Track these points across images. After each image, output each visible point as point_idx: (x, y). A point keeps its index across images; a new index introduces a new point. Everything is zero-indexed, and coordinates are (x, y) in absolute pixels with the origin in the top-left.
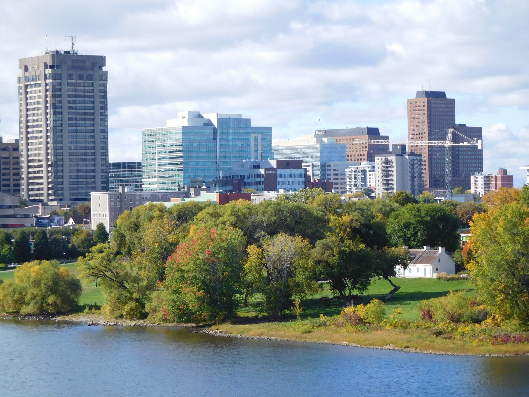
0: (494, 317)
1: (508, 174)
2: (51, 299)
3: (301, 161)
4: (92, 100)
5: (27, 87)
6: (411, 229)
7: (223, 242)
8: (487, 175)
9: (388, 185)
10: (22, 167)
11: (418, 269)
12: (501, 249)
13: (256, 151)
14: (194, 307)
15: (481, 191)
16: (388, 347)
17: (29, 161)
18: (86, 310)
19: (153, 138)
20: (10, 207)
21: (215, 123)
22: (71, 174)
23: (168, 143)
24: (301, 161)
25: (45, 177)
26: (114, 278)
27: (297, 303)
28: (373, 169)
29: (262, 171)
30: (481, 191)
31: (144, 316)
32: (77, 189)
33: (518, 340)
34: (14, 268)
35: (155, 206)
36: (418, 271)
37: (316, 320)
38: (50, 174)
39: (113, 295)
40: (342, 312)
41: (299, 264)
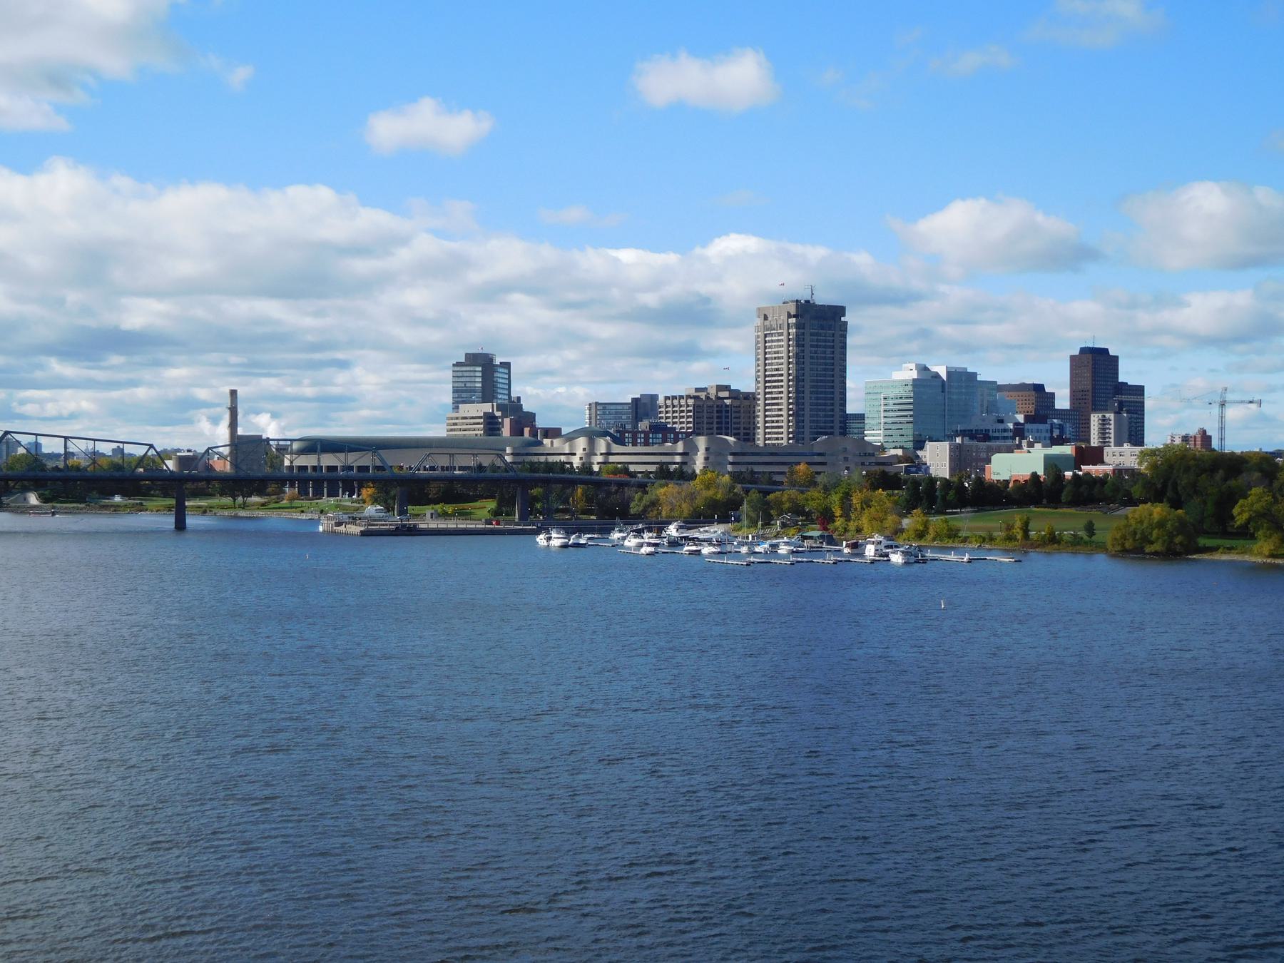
2: (1178, 539)
5: (766, 336)
9: (1105, 442)
10: (758, 416)
18: (1221, 550)
20: (819, 454)
21: (944, 376)
25: (785, 427)
38: (791, 424)
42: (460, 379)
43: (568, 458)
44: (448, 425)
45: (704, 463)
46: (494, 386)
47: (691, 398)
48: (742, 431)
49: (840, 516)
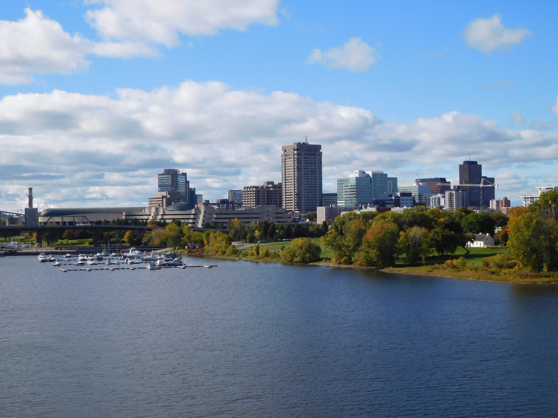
0: (519, 265)
1: (508, 200)
2: (308, 255)
3: (412, 193)
4: (315, 165)
5: (285, 159)
6: (473, 225)
7: (389, 230)
8: (498, 200)
9: (452, 204)
11: (477, 243)
12: (523, 234)
13: (390, 189)
14: (375, 259)
15: (495, 207)
16: (470, 279)
17: (286, 193)
19: (342, 182)
21: (371, 176)
22: (305, 199)
23: (349, 185)
24: (412, 193)
25: (293, 200)
26: (337, 246)
27: (423, 258)
28: (444, 197)
29: (393, 198)
30: (495, 207)
31: (351, 263)
32: (308, 205)
33: (532, 277)
34: (291, 240)
35: (352, 213)
36: (477, 244)
37: (433, 266)
38: (296, 199)
39: (336, 253)
40: (445, 263)
41: (424, 240)
42: (162, 181)
43: (148, 217)
44: (149, 201)
45: (203, 218)
46: (177, 184)
47: (255, 188)
48: (278, 202)
49: (207, 244)
